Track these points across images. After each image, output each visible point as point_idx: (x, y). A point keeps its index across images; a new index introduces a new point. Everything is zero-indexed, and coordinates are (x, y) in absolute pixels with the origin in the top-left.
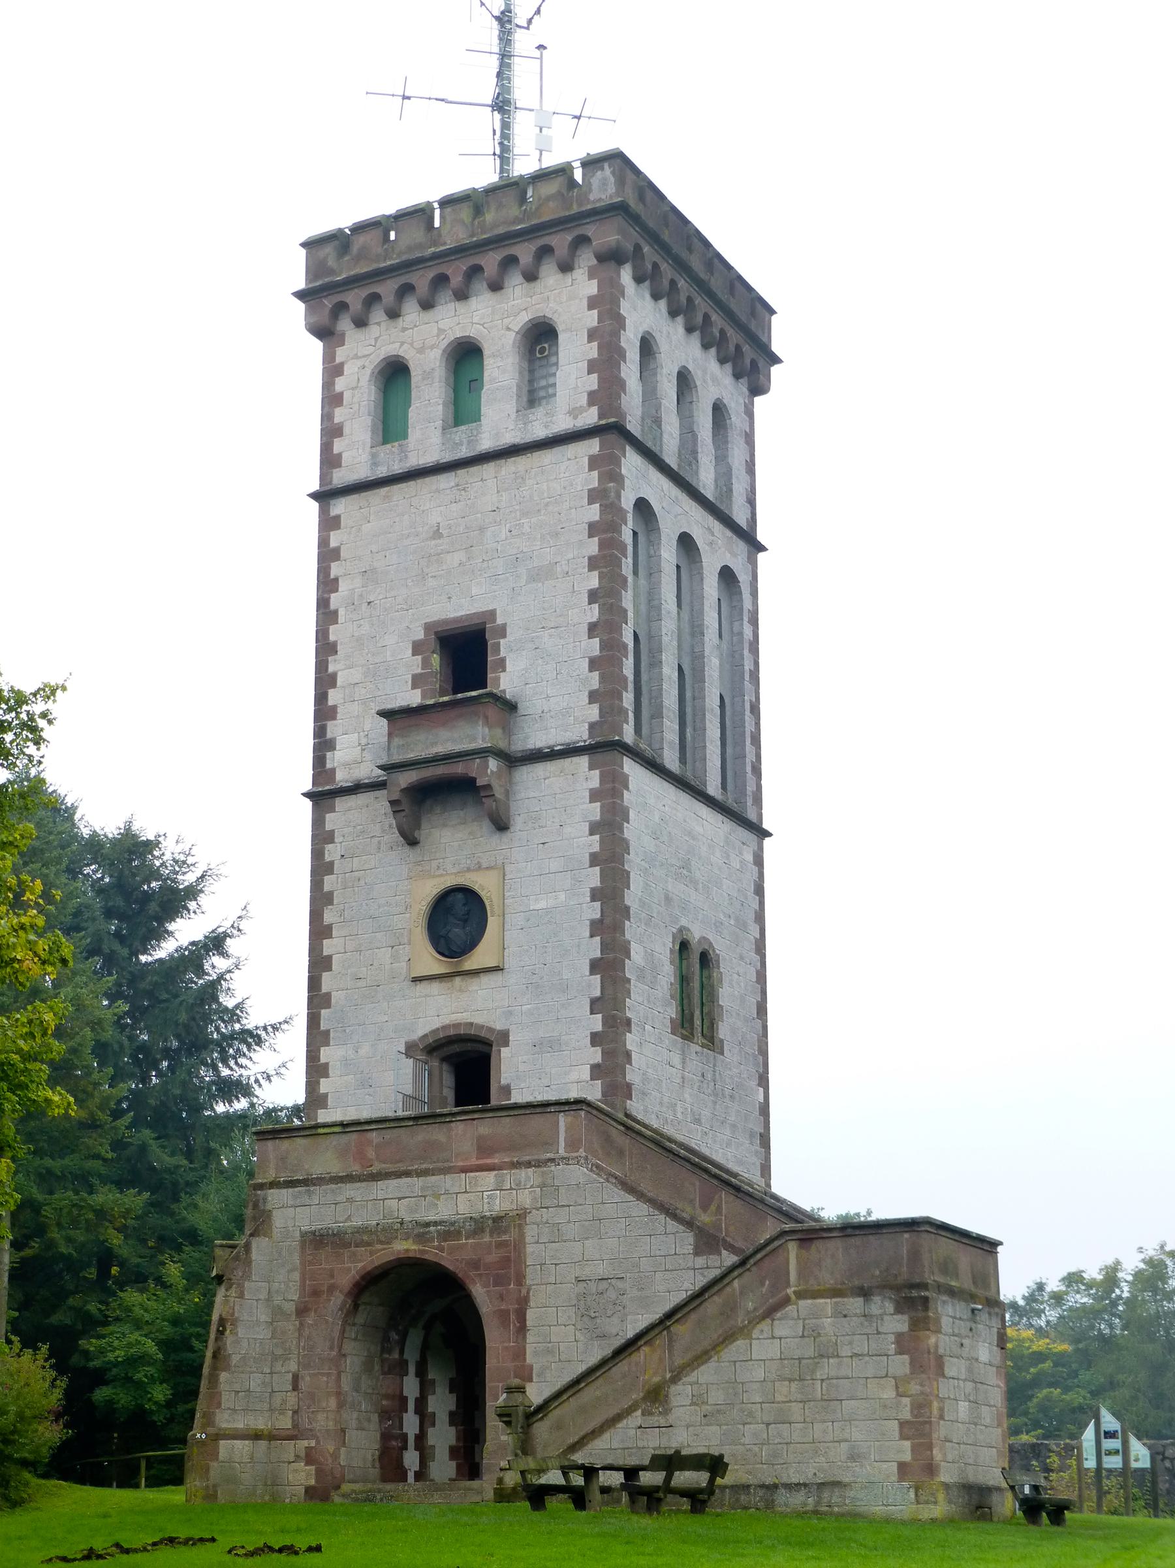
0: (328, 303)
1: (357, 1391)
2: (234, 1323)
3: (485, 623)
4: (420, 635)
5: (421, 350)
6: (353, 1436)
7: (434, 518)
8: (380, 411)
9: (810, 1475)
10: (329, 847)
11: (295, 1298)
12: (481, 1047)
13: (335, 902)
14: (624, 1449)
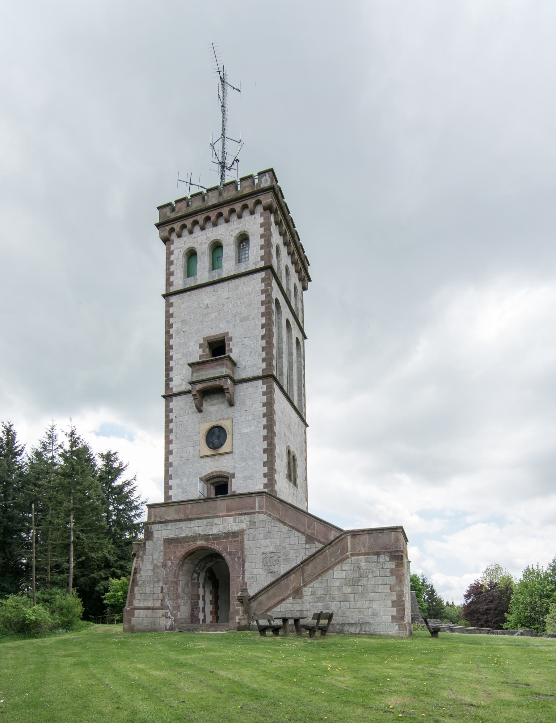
0: (168, 228)
1: (183, 593)
2: (140, 569)
3: (224, 337)
4: (202, 342)
5: (201, 245)
6: (182, 608)
7: (207, 301)
8: (187, 268)
9: (357, 620)
10: (171, 414)
11: (162, 561)
12: (224, 479)
13: (173, 432)
14: (285, 611)
